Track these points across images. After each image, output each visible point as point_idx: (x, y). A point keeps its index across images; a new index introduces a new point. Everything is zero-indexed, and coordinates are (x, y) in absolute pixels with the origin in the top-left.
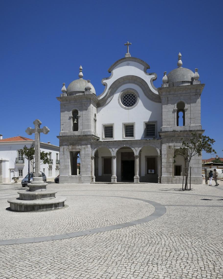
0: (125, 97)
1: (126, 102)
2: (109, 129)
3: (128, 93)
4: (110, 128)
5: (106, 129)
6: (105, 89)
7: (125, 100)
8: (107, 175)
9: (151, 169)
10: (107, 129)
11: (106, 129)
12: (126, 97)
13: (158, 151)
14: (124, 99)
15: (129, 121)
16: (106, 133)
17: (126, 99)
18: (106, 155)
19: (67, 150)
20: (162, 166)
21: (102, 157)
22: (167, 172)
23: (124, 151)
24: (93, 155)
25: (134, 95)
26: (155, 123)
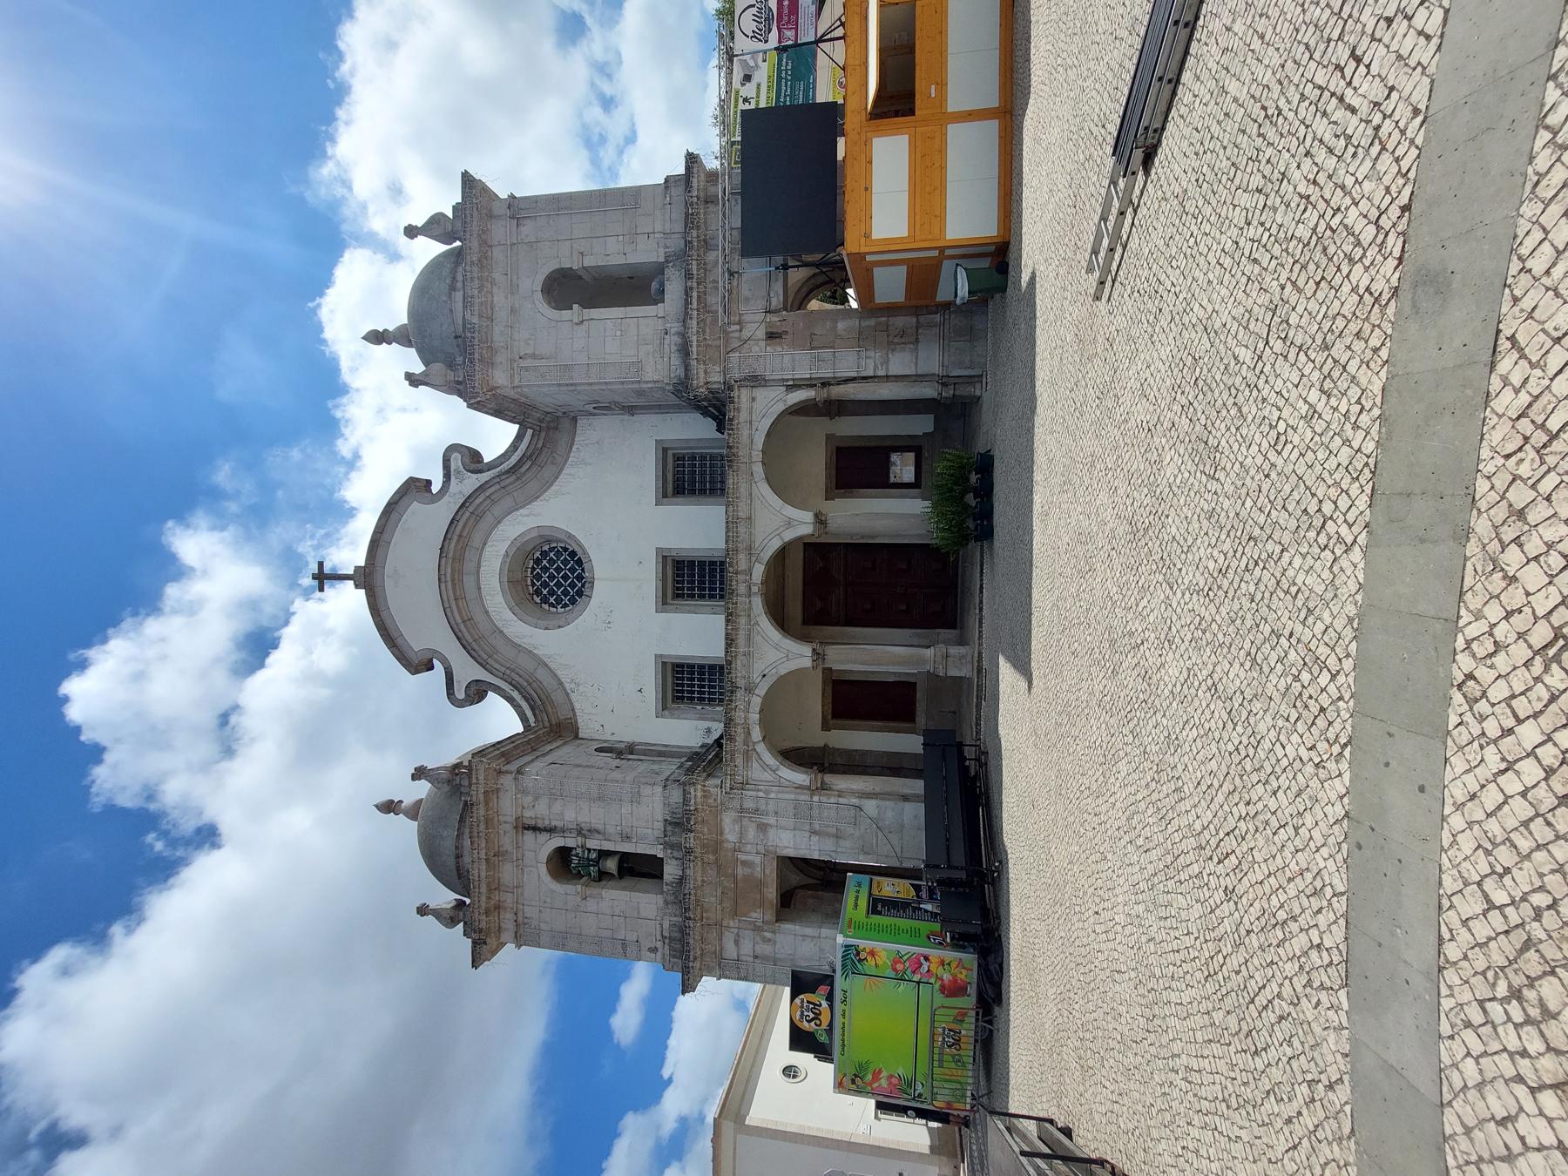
0: (545, 600)
1: (565, 593)
2: (688, 686)
3: (529, 583)
4: (683, 685)
5: (688, 698)
6: (874, 723)
7: (558, 601)
8: (921, 708)
9: (886, 465)
10: (688, 686)
11: (688, 698)
12: (545, 592)
13: (796, 400)
14: (552, 605)
15: (648, 579)
16: (704, 699)
17: (552, 593)
18: (814, 702)
19: (768, 935)
20: (881, 373)
21: (826, 727)
22: (917, 341)
23: (795, 608)
24: (800, 777)
25: (538, 554)
26: (670, 453)
